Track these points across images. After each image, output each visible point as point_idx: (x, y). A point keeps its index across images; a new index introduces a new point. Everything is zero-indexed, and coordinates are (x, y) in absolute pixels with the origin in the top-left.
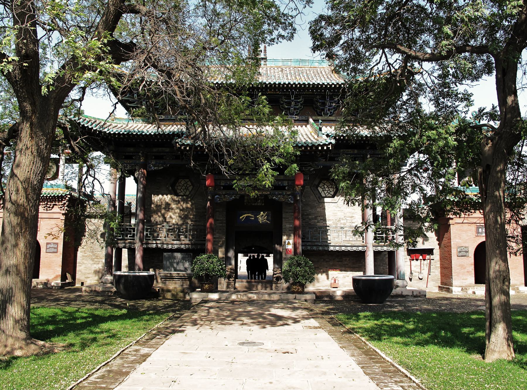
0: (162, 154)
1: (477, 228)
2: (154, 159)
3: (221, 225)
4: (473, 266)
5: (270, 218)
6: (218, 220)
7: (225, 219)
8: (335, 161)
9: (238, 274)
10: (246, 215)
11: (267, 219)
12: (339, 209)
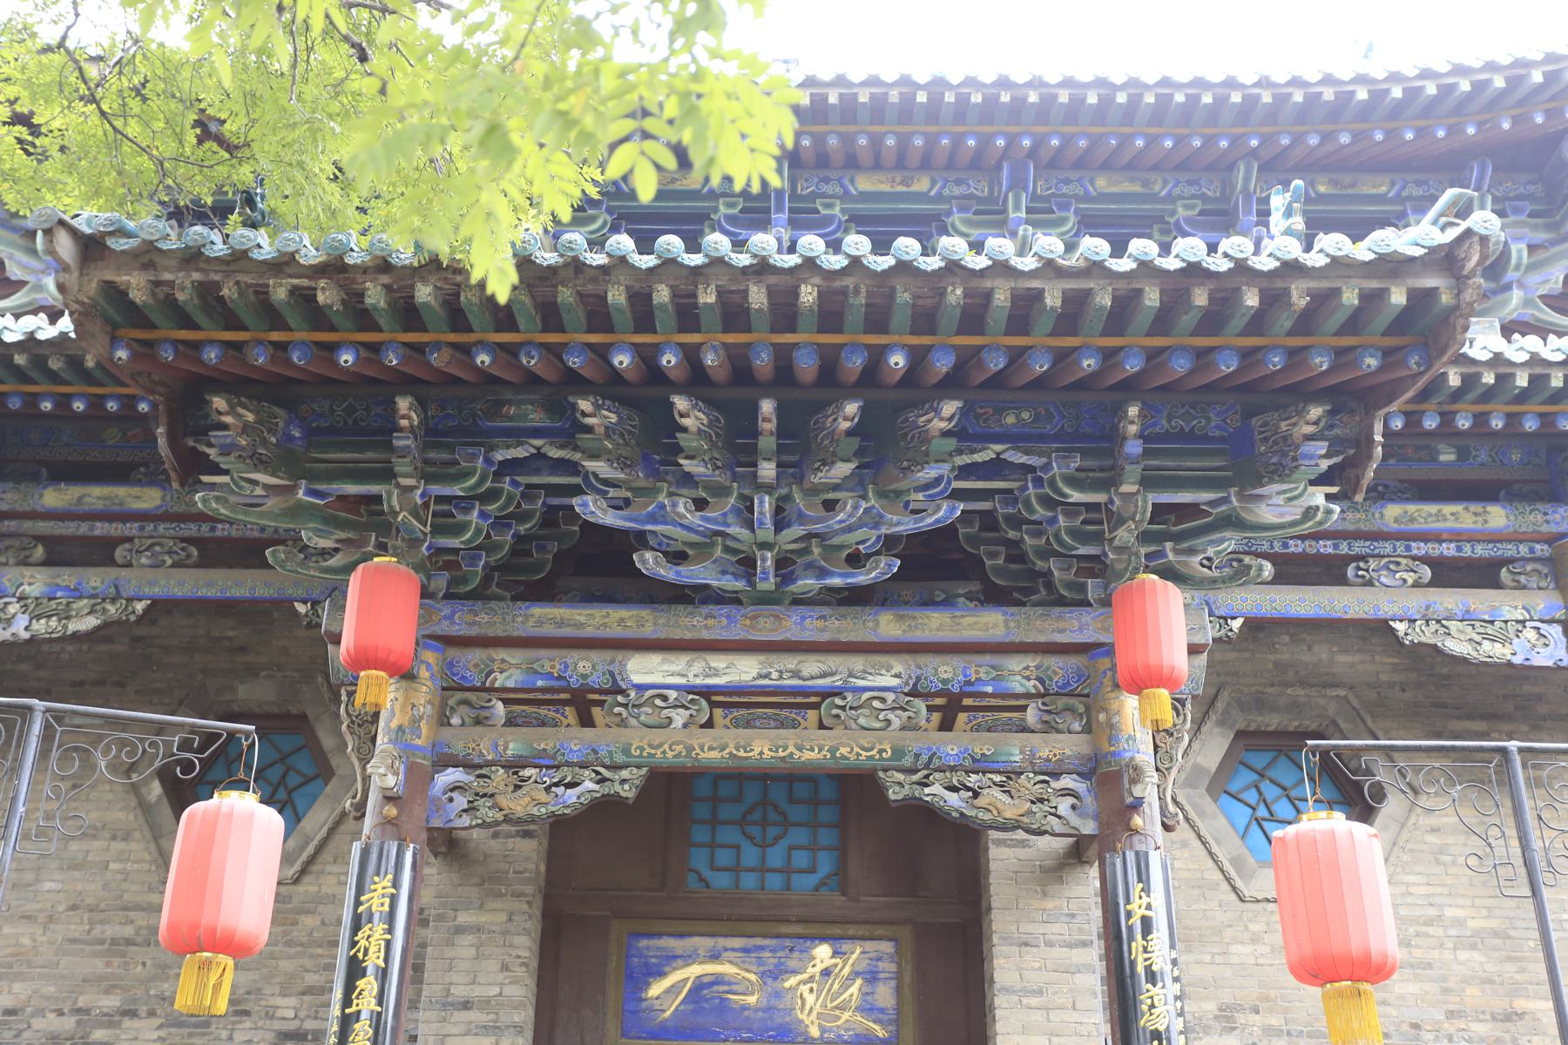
0: (100, 529)
2: (47, 563)
5: (885, 995)
6: (466, 1005)
8: (1342, 580)
10: (695, 970)
11: (867, 1009)
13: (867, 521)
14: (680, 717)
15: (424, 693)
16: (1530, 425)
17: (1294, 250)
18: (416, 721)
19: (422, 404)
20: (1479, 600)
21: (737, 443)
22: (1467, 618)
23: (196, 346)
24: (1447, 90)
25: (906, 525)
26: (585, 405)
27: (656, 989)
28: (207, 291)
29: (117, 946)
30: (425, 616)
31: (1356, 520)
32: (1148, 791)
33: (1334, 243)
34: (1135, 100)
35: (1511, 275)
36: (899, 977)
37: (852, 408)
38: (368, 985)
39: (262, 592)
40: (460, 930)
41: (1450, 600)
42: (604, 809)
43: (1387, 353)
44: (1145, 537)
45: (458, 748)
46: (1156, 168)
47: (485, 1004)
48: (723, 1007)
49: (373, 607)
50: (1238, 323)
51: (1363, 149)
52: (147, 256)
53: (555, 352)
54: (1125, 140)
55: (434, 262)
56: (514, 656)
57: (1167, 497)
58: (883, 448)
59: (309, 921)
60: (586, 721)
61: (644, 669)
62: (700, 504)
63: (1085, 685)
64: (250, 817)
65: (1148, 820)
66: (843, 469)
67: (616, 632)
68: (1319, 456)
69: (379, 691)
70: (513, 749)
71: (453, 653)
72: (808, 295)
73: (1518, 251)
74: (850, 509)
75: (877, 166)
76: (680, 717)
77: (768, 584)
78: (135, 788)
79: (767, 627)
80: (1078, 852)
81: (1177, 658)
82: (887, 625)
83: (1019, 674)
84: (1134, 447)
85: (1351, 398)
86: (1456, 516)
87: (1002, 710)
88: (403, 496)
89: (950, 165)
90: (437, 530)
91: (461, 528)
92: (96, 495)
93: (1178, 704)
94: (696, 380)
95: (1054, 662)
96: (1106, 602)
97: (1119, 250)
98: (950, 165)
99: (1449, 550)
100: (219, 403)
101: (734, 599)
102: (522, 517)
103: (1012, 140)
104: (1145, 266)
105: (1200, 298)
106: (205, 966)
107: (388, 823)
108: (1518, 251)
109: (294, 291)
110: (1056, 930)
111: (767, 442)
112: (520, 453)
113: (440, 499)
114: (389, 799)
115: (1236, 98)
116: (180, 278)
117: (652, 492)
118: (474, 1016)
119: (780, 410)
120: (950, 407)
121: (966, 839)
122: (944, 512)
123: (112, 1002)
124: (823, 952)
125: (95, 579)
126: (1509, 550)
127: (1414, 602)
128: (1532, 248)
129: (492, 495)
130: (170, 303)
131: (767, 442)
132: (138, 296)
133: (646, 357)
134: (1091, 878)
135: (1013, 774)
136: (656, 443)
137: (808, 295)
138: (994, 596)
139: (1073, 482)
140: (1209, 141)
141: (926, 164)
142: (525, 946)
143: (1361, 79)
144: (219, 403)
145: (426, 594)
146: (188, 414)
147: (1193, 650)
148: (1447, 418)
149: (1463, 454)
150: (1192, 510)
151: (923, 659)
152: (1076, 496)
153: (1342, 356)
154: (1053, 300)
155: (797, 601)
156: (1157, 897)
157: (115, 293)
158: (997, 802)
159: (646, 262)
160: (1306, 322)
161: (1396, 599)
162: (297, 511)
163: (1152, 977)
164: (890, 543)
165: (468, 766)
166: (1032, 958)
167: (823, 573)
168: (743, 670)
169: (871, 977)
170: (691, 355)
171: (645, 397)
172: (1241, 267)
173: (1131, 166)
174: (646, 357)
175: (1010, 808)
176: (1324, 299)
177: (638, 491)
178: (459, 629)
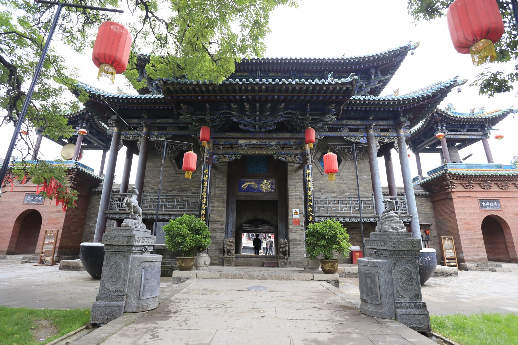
0: (165, 125)
1: (480, 202)
2: (158, 130)
3: (221, 192)
4: (483, 241)
5: (274, 186)
6: (218, 187)
7: (224, 186)
8: (338, 131)
9: (129, 183)
10: (248, 183)
11: (271, 188)
12: (343, 182)
13: (272, 121)
14: (246, 148)
15: (211, 145)
16: (363, 109)
17: (331, 81)
18: (210, 149)
19: (209, 105)
20: (356, 134)
21: (253, 109)
22: (354, 136)
23: (179, 97)
24: (354, 61)
25: (276, 121)
26: (232, 104)
27: (243, 186)
28: (181, 88)
29: (171, 182)
30: (211, 135)
31: (339, 122)
32: (309, 157)
33: (336, 80)
34: (310, 62)
35: (363, 88)
36: (276, 184)
37: (269, 105)
38: (206, 182)
39: (187, 134)
40: (217, 178)
41: (352, 134)
42: (236, 160)
43: (343, 96)
44: (310, 123)
45: (216, 152)
46: (313, 72)
47: (220, 187)
48: (252, 188)
49: (204, 133)
50: (323, 92)
51: (340, 67)
52: (173, 83)
53: (228, 96)
54: (309, 68)
55: (212, 84)
56: (223, 140)
57: (313, 117)
58: (274, 111)
59: (195, 179)
60: (232, 149)
61: (241, 142)
62: (248, 118)
63: (302, 142)
64: (193, 154)
65: (309, 161)
66: (268, 113)
67: (237, 136)
68: (334, 111)
69: (205, 143)
70: (223, 152)
71: (215, 140)
72: (263, 87)
73: (364, 85)
74: (269, 119)
75: (273, 72)
76: (246, 148)
77: (258, 130)
78: (171, 161)
79: (258, 136)
80: (300, 167)
81: (314, 138)
82: (275, 135)
83: (292, 142)
84: (308, 110)
85: (338, 103)
86: (353, 122)
87: (290, 147)
88: (208, 118)
89: (284, 71)
90: (212, 123)
91: (215, 122)
92: (164, 120)
93: (314, 146)
94: (248, 101)
95: (297, 141)
96: (304, 132)
97: (307, 81)
98: (284, 71)
99: (352, 127)
100: (182, 105)
101: (253, 132)
102: (223, 121)
103: (292, 68)
104: (310, 83)
105: (318, 88)
106: (188, 173)
107: (207, 162)
108: (364, 85)
109: (192, 88)
110: (297, 177)
111: (258, 109)
112: (223, 112)
113: (212, 118)
114: (207, 159)
115: (325, 61)
116: (177, 87)
117: (242, 117)
118: (219, 189)
119: (259, 105)
120: (283, 105)
121: (284, 165)
122: (282, 119)
123: (171, 189)
124: (265, 181)
125: (164, 132)
126: (360, 127)
127: (347, 134)
128: (366, 85)
129: (219, 118)
130: (176, 90)
131: (258, 109)
132: (171, 89)
133: (241, 97)
134: (301, 172)
135: (291, 155)
136: (242, 110)
137: (263, 87)
138: (289, 132)
139: (300, 115)
140: (321, 68)
141: (280, 71)
142: (225, 180)
143: (342, 59)
144: (182, 105)
145: (211, 132)
146: (178, 107)
147: (316, 139)
148: (352, 108)
149: (355, 113)
150: (316, 119)
151: (280, 140)
152: (300, 117)
153: (337, 97)
154: (297, 88)
155: (262, 132)
156: (310, 171)
157: (168, 89)
158: (289, 159)
159: (241, 83)
160: (332, 92)
161: (344, 134)
162: (193, 120)
163: (309, 181)
164: (275, 124)
165: (217, 155)
166: (293, 181)
167: (266, 128)
168: (255, 142)
169: (272, 184)
170: (247, 96)
171: (240, 103)
172: (323, 83)
173: (309, 72)
174: (241, 97)
175: (291, 160)
176: (335, 88)
177: (240, 117)
178: (215, 136)
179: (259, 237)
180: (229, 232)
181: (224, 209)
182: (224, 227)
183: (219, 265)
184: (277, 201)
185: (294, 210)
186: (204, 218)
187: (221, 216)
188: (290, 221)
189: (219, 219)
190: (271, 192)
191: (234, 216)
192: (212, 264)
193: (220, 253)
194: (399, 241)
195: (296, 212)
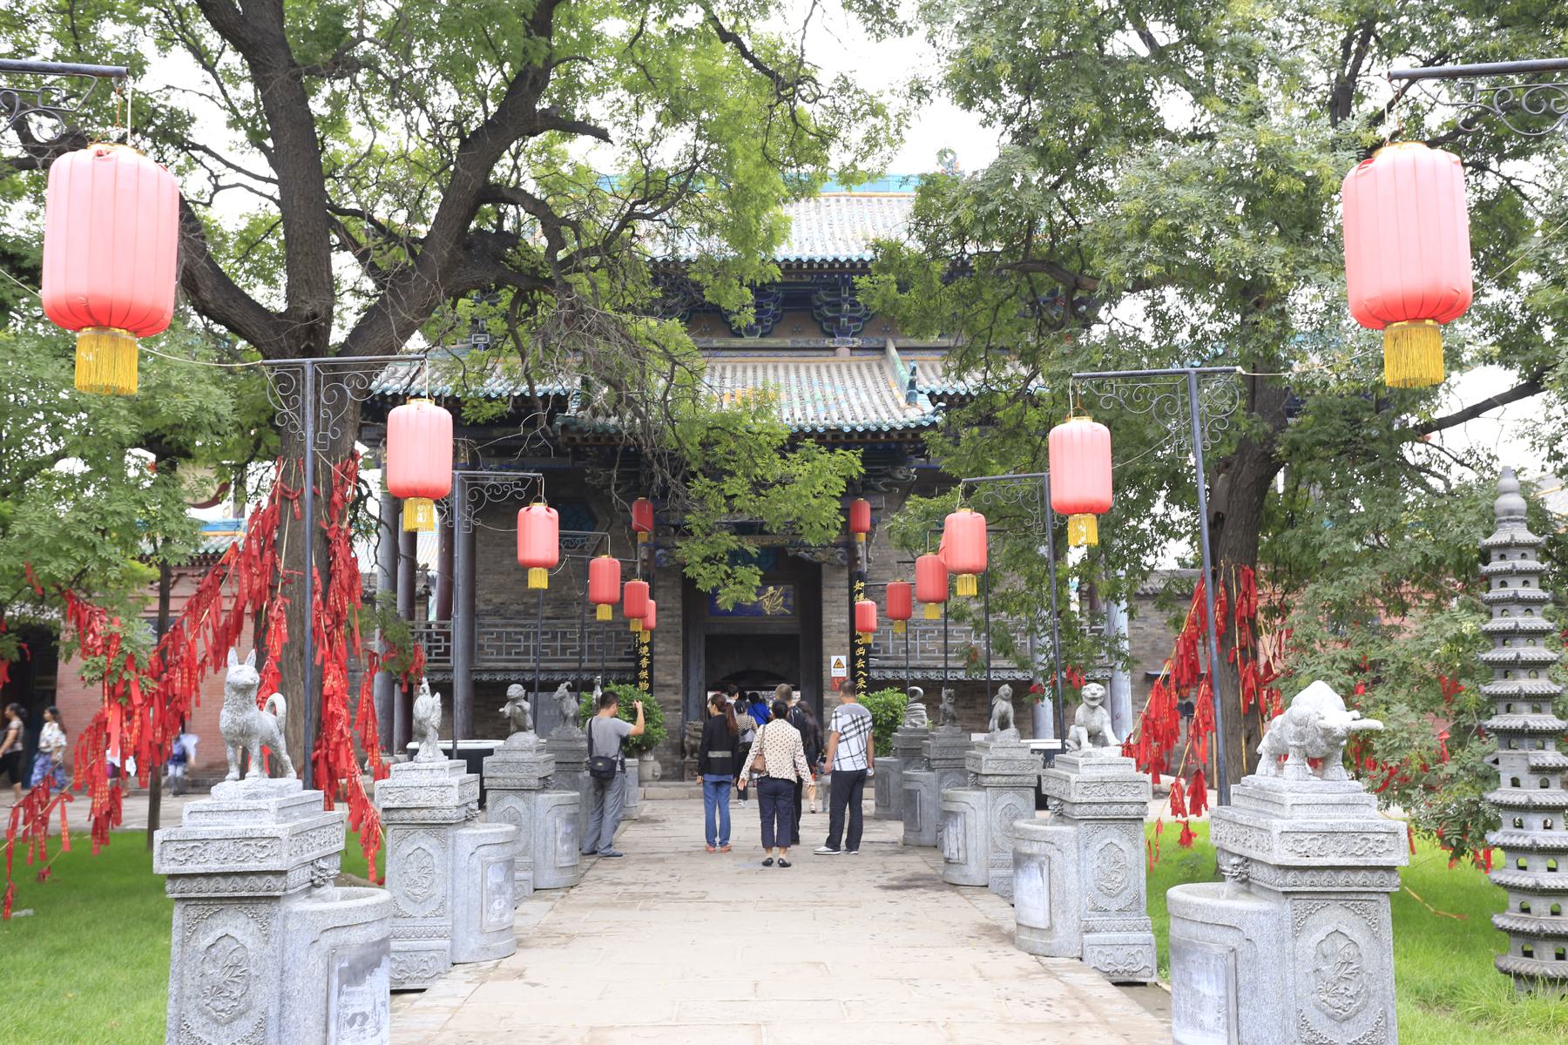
5: (790, 601)
11: (785, 605)
169: (786, 596)
179: (780, 259)
180: (691, 707)
181: (679, 658)
182: (680, 697)
183: (673, 779)
184: (797, 636)
185: (834, 659)
186: (647, 686)
187: (674, 674)
188: (826, 682)
189: (669, 680)
190: (784, 614)
191: (702, 672)
192: (663, 778)
193: (675, 753)
194: (912, 739)
195: (838, 663)
